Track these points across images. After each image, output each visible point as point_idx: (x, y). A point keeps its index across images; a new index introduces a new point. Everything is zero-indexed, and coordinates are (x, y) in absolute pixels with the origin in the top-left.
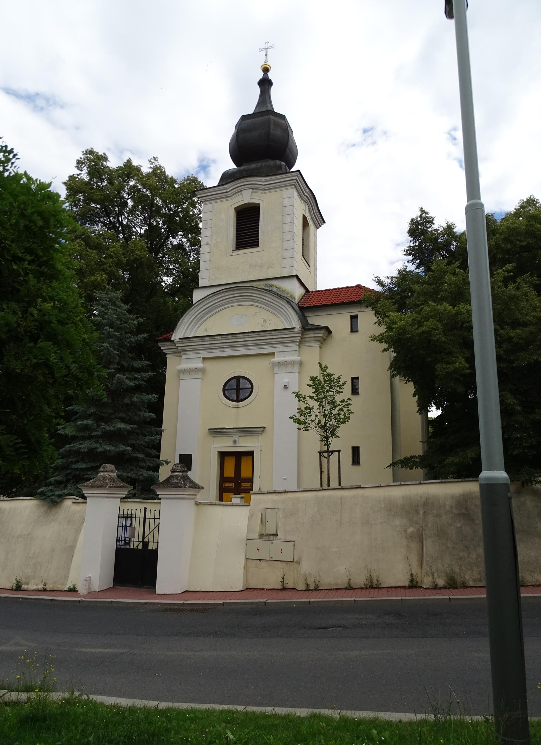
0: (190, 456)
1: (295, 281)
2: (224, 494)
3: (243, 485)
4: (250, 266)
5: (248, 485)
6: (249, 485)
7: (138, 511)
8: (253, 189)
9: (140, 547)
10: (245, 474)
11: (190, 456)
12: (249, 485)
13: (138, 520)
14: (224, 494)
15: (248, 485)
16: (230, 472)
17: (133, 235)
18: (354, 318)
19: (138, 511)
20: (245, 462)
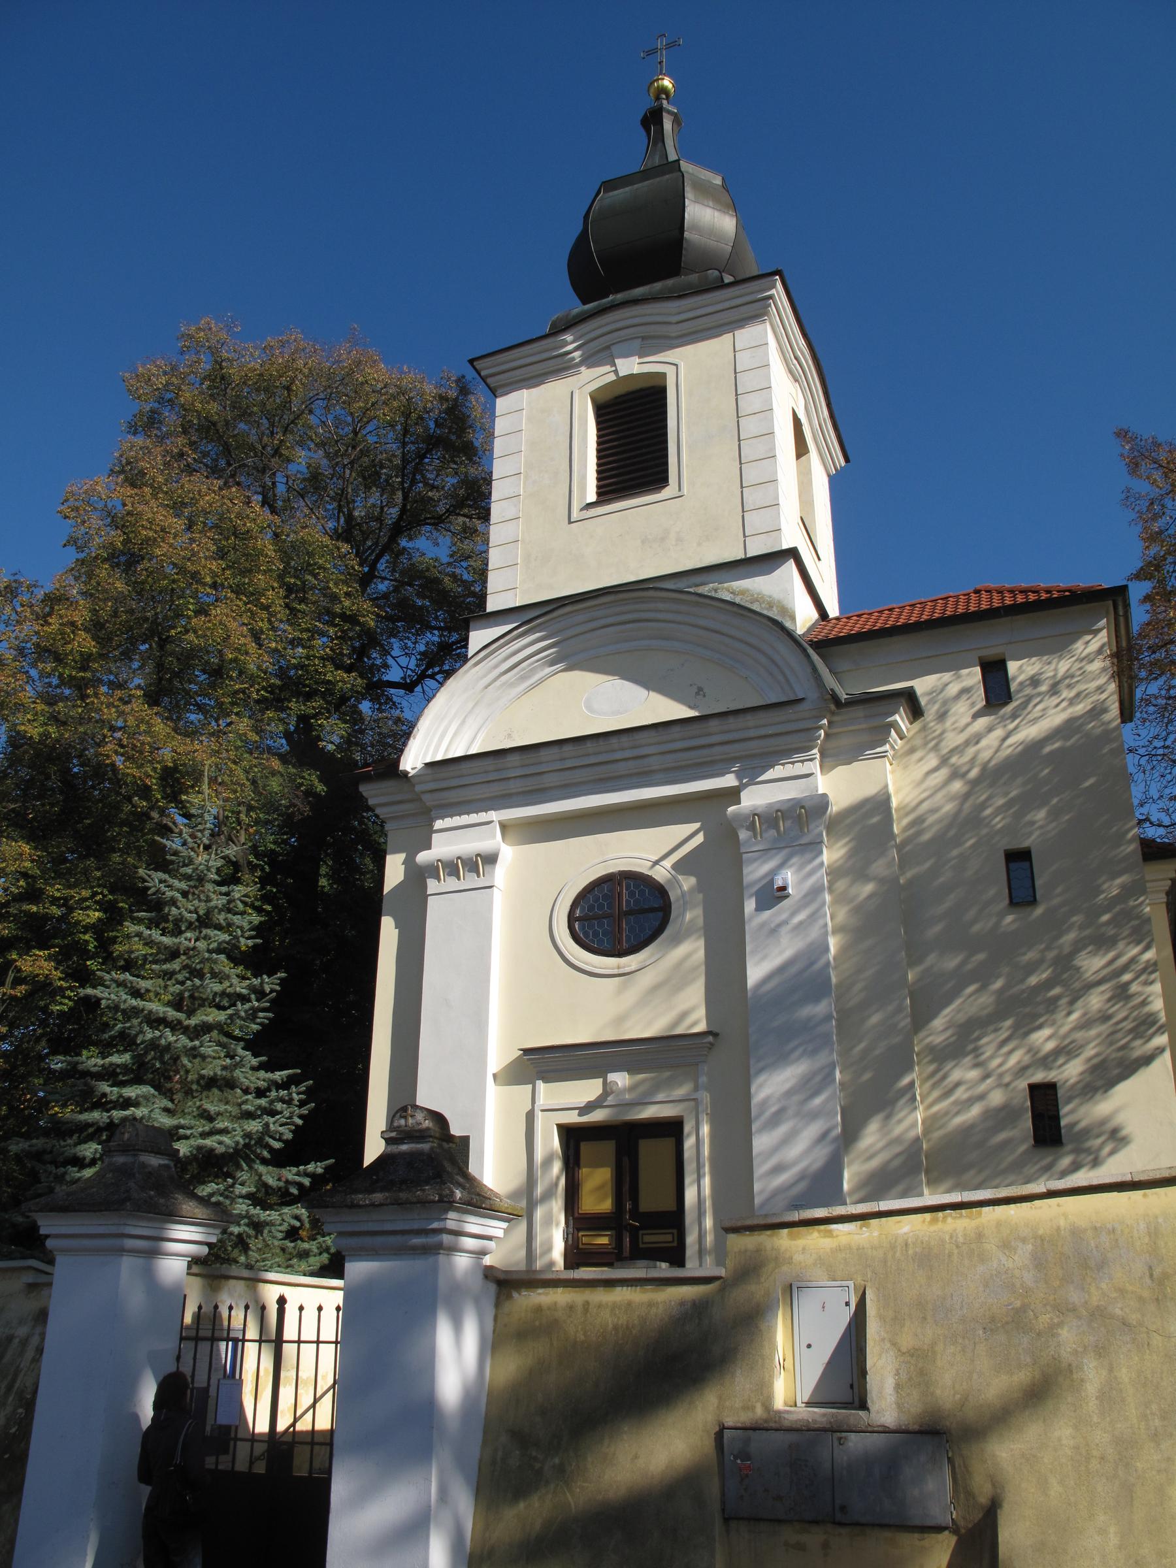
0: (468, 1137)
1: (791, 564)
2: (675, 1209)
3: (647, 1239)
4: (643, 542)
5: (663, 1238)
6: (669, 1238)
7: (310, 1315)
8: (643, 338)
9: (260, 1468)
10: (652, 1200)
11: (468, 1137)
12: (669, 1238)
13: (308, 1351)
14: (675, 1209)
15: (663, 1238)
16: (598, 1197)
17: (271, 1150)
18: (994, 671)
19: (310, 1315)
20: (650, 1151)
